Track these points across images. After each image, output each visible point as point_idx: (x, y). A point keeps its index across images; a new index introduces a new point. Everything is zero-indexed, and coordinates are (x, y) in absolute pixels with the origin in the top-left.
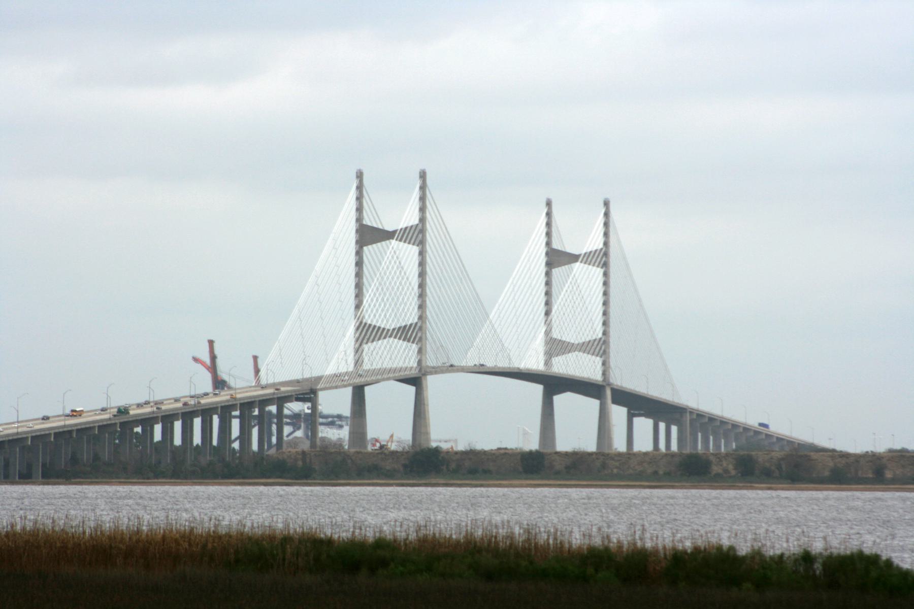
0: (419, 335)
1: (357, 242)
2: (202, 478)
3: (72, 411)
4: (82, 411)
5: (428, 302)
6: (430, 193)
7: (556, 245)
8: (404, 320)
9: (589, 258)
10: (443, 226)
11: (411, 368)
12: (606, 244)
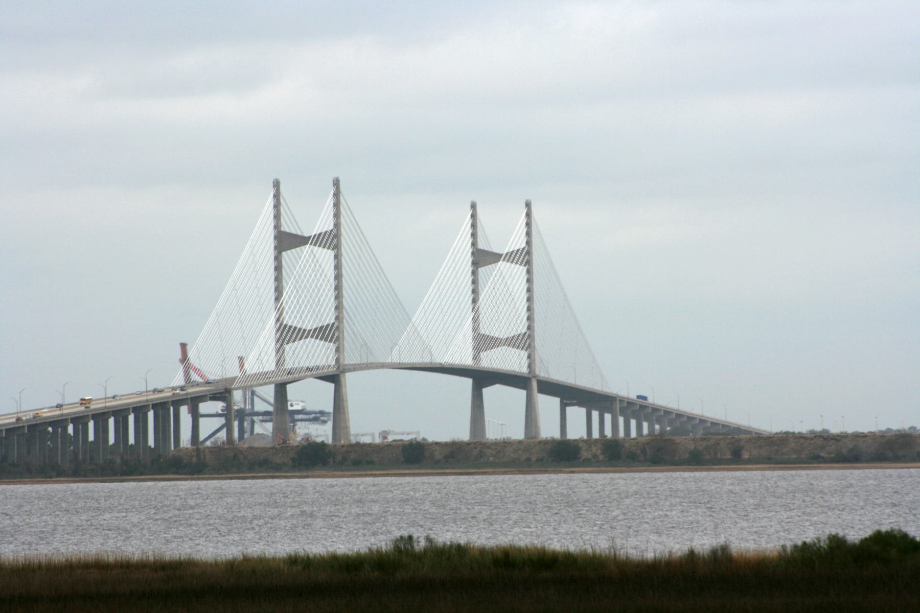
0: (336, 335)
1: (275, 248)
2: (102, 476)
3: (82, 400)
4: (91, 399)
5: (344, 303)
6: (344, 198)
7: (481, 245)
8: (320, 320)
9: (511, 257)
10: (359, 231)
11: (329, 366)
12: (528, 243)
